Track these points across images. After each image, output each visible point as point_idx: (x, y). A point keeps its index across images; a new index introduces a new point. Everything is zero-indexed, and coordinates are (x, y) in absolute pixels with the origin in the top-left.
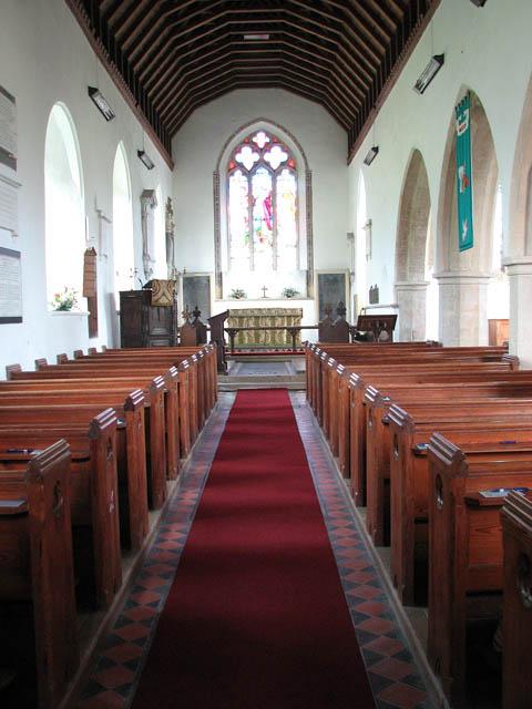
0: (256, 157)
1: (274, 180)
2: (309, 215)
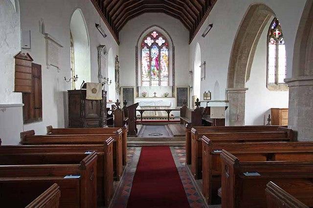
0: (153, 41)
1: (160, 51)
2: (173, 64)
